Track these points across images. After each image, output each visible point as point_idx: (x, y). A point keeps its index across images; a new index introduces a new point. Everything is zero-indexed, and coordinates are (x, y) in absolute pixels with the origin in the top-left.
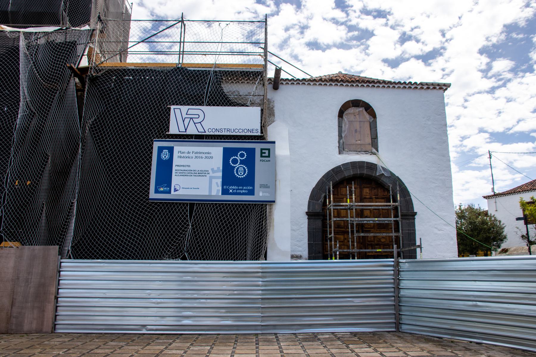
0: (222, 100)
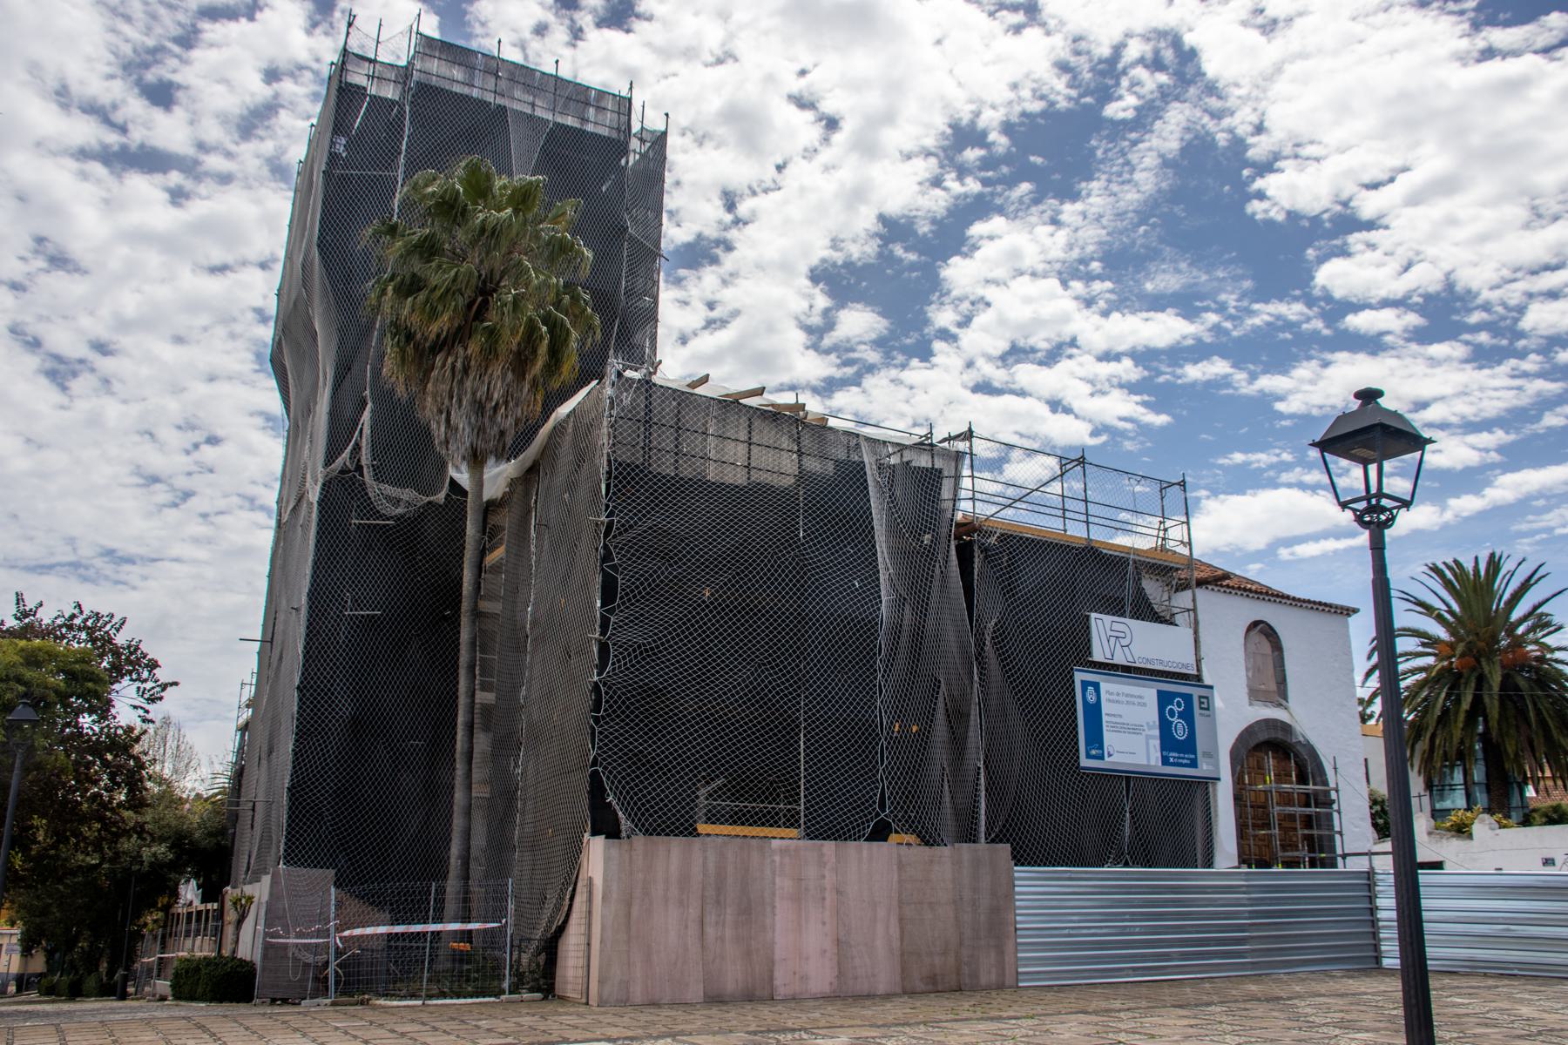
0: (1145, 611)
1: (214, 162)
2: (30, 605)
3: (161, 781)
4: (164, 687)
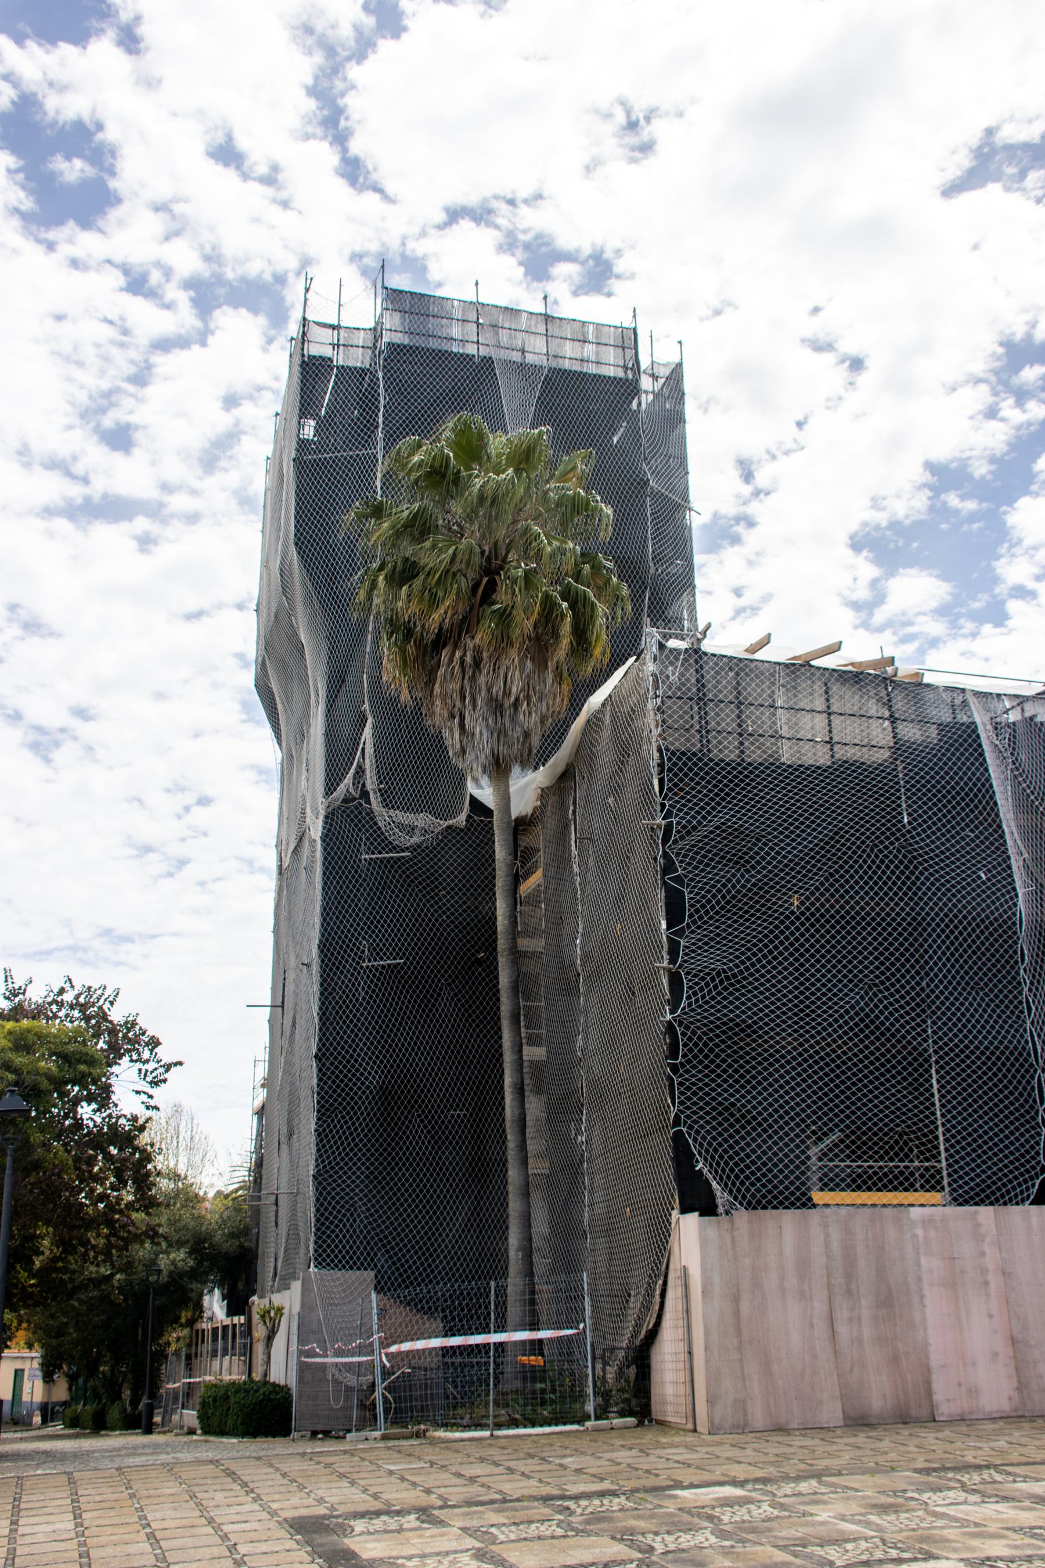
1: (179, 502)
2: (19, 982)
3: (176, 1177)
4: (168, 1067)
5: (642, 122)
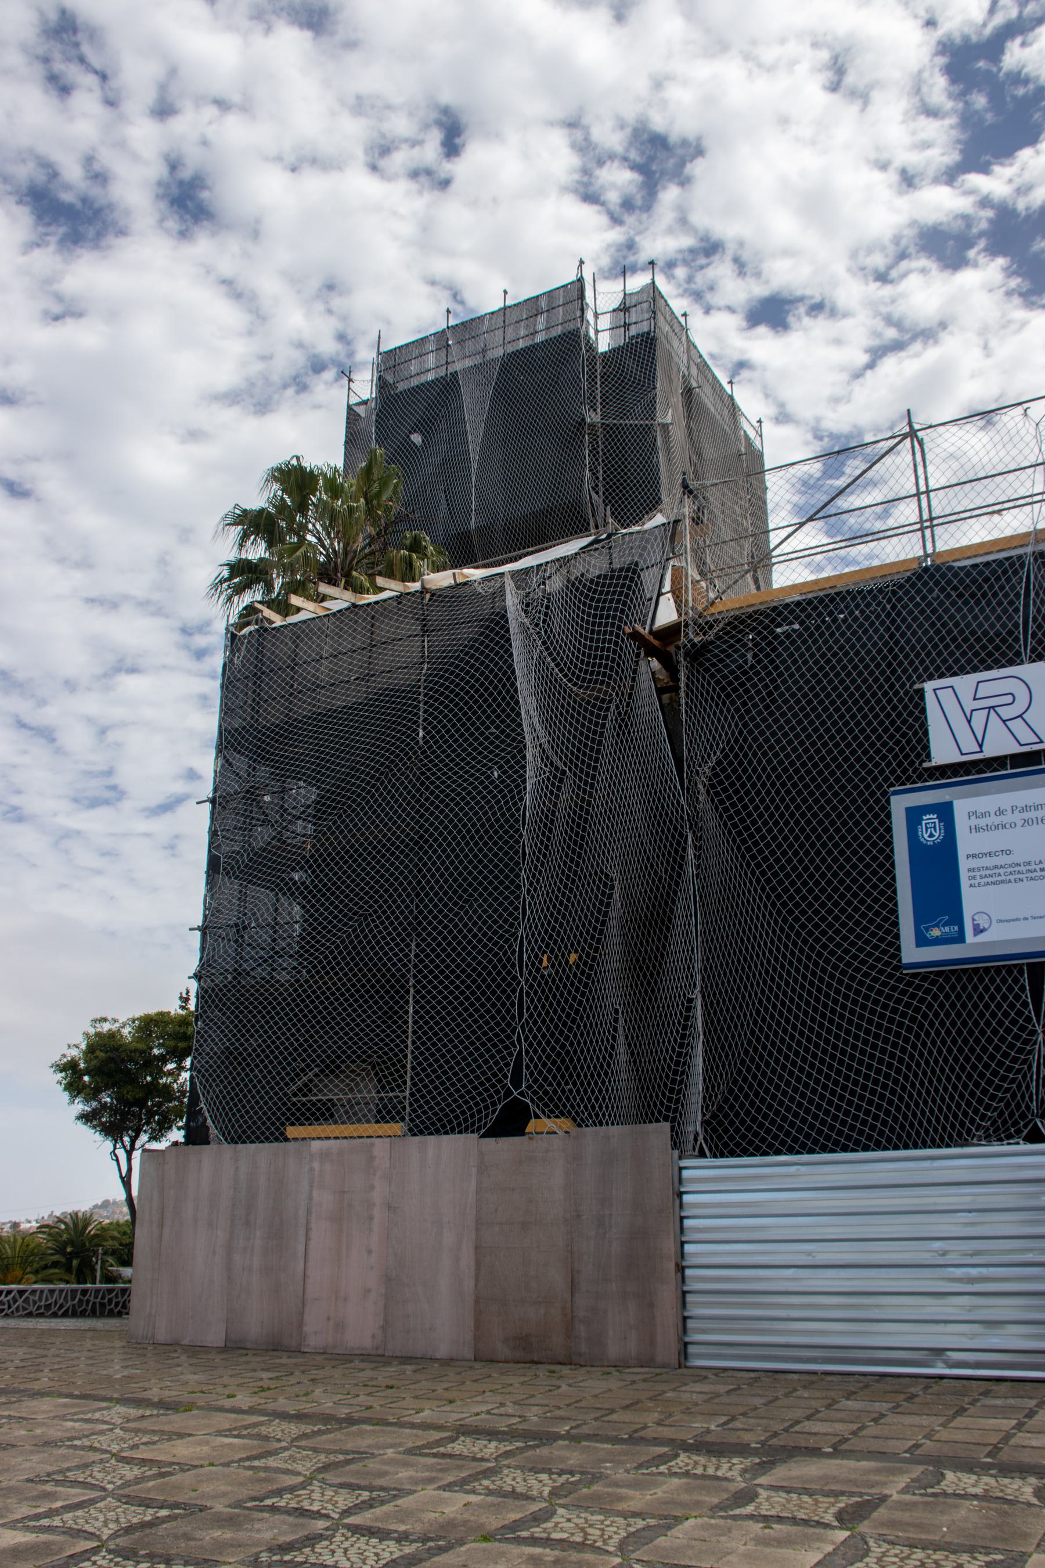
5: (95, 191)
